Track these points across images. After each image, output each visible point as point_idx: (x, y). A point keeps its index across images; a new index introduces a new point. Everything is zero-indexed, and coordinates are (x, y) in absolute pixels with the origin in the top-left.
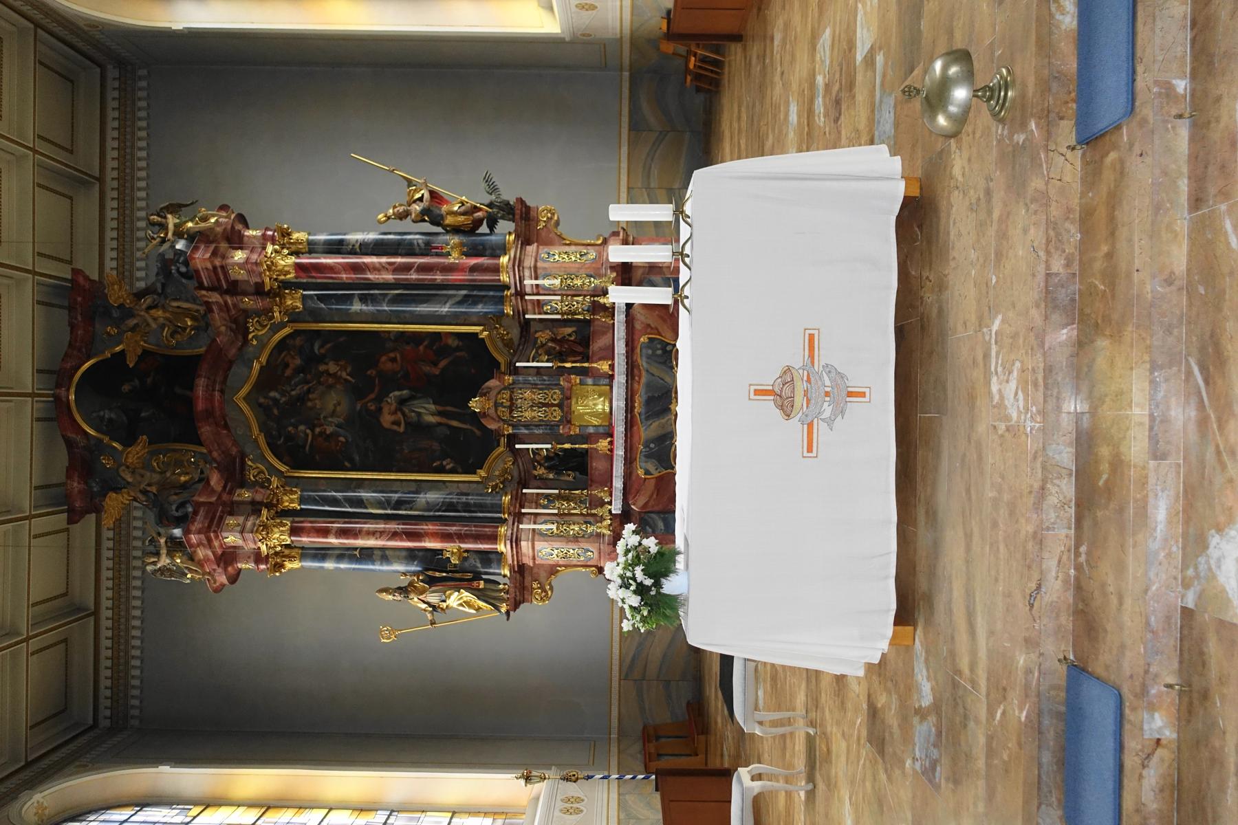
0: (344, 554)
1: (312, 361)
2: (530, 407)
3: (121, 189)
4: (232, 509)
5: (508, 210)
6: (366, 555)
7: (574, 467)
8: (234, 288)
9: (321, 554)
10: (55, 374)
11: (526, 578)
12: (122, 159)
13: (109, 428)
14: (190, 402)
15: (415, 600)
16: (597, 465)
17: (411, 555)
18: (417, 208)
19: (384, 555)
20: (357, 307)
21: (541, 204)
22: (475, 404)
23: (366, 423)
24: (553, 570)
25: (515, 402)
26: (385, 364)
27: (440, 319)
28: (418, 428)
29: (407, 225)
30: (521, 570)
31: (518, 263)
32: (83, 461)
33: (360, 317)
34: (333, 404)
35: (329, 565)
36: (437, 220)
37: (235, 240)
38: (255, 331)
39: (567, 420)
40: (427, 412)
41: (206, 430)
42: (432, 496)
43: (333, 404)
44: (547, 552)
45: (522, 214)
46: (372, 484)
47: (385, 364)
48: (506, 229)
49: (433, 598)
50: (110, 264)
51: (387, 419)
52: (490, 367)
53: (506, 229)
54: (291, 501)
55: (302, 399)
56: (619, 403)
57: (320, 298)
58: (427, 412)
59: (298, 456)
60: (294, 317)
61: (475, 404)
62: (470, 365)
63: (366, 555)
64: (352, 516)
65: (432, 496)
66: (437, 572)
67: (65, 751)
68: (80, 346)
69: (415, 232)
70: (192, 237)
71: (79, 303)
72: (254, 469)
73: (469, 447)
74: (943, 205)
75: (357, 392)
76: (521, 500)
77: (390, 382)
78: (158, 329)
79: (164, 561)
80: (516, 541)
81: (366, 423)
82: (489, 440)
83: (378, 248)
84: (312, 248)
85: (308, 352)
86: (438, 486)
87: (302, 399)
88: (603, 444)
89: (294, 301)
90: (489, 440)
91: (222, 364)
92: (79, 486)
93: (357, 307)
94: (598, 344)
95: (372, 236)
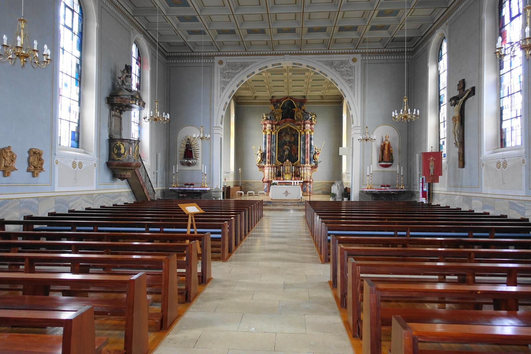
0: (265, 141)
1: (294, 135)
2: (287, 168)
3: (321, 102)
4: (272, 125)
5: (316, 165)
6: (265, 144)
7: (279, 175)
8: (304, 124)
9: (265, 137)
10: (291, 98)
11: (262, 168)
12: (326, 102)
13: (284, 105)
14: (287, 118)
15: (259, 152)
16: (279, 178)
17: (265, 151)
18: (317, 151)
19: (265, 147)
20: (302, 143)
21: (318, 169)
22: (288, 160)
23: (285, 143)
24: (264, 172)
25: (288, 166)
26: (294, 146)
27: (300, 155)
28: (284, 151)
29: (314, 149)
30: (264, 167)
31: (308, 167)
32: (279, 101)
33: (300, 142)
34: (287, 139)
35: (264, 139)
36: (315, 154)
37: (311, 124)
38: (298, 127)
39: (285, 174)
40: (287, 153)
41: (283, 120)
42: (274, 154)
43: (287, 139)
44: (266, 171)
45: (316, 167)
46: (276, 145)
47: (294, 146)
48: (313, 164)
49: (259, 154)
50: (309, 101)
51: (285, 147)
52: (293, 162)
53: (313, 164)
54: (273, 133)
55: (288, 134)
56: (288, 181)
57: (60, 237)
58: (287, 153)
59: (279, 133)
60: (300, 133)
61: (288, 160)
62: (293, 158)
63: (265, 144)
64: (271, 143)
65: (274, 154)
66: (263, 155)
67: (151, 38)
68: (296, 100)
69: (313, 151)
70: (311, 119)
71: (303, 101)
72: (278, 127)
73: (281, 159)
74: (350, 339)
75: (289, 142)
76: (274, 167)
77: (291, 147)
78: (298, 114)
79: (265, 116)
80: (268, 167)
81: (285, 143)
82: (283, 162)
83: (311, 145)
84: (311, 135)
85: (295, 135)
86: (275, 155)
87: (288, 134)
88: (282, 179)
89: (303, 133)
90: (283, 162)
91: (294, 122)
92: (275, 102)
93: (302, 143)
94: (296, 178)
95: (313, 144)
